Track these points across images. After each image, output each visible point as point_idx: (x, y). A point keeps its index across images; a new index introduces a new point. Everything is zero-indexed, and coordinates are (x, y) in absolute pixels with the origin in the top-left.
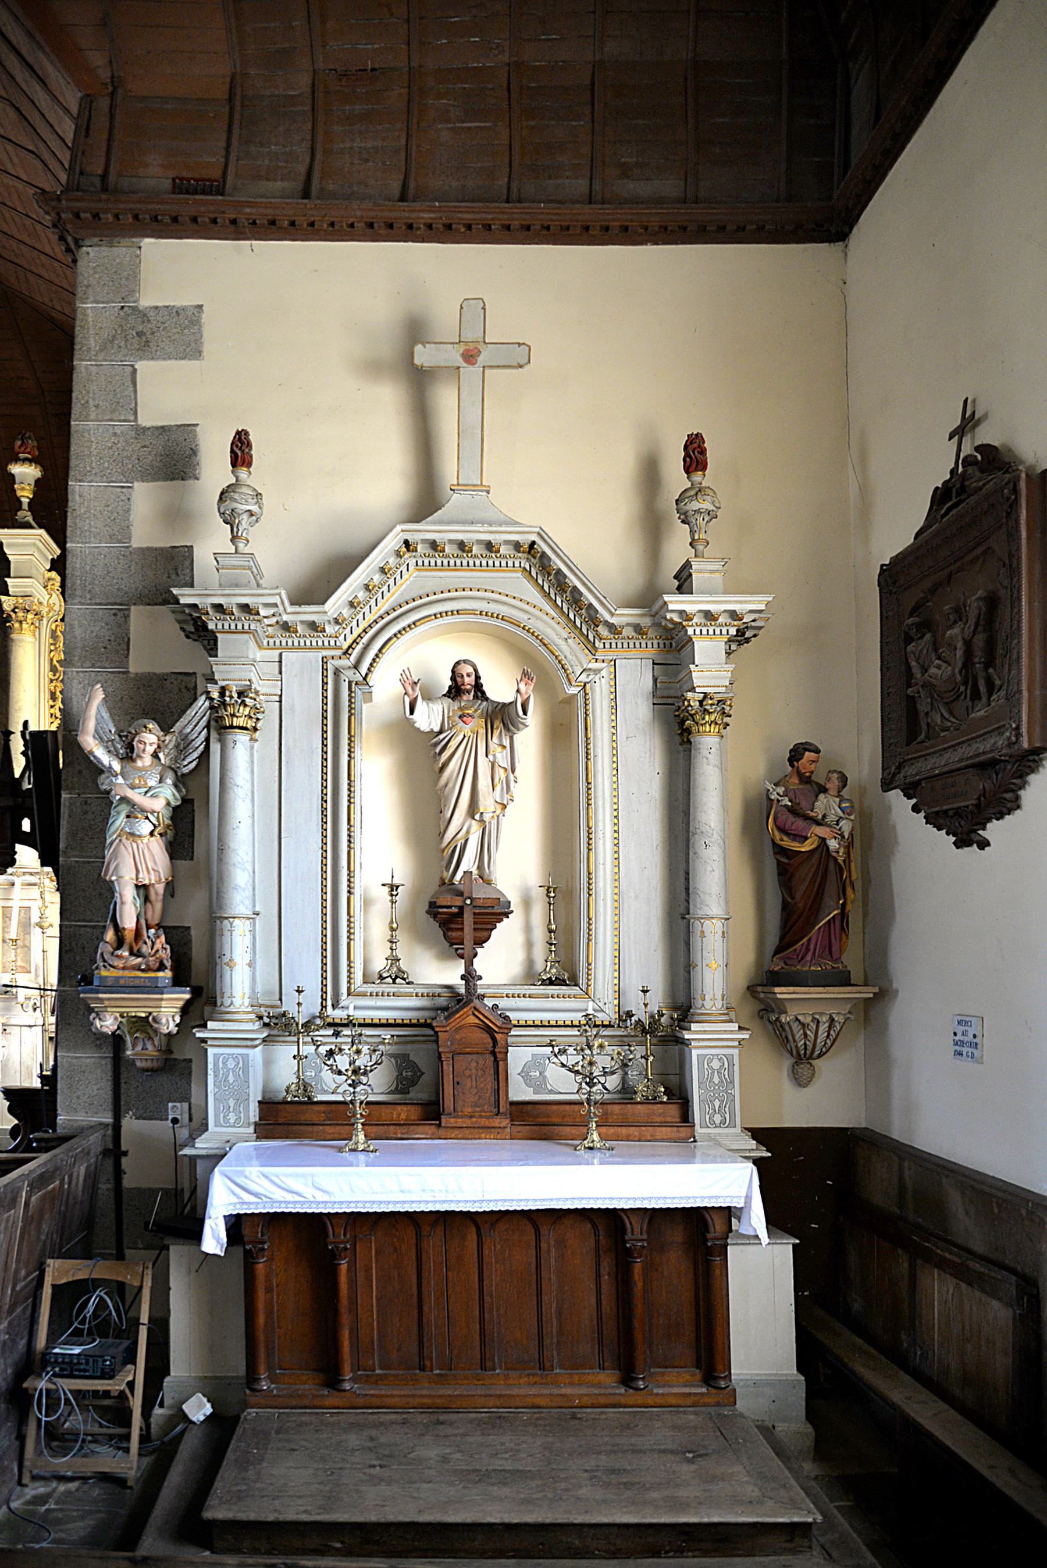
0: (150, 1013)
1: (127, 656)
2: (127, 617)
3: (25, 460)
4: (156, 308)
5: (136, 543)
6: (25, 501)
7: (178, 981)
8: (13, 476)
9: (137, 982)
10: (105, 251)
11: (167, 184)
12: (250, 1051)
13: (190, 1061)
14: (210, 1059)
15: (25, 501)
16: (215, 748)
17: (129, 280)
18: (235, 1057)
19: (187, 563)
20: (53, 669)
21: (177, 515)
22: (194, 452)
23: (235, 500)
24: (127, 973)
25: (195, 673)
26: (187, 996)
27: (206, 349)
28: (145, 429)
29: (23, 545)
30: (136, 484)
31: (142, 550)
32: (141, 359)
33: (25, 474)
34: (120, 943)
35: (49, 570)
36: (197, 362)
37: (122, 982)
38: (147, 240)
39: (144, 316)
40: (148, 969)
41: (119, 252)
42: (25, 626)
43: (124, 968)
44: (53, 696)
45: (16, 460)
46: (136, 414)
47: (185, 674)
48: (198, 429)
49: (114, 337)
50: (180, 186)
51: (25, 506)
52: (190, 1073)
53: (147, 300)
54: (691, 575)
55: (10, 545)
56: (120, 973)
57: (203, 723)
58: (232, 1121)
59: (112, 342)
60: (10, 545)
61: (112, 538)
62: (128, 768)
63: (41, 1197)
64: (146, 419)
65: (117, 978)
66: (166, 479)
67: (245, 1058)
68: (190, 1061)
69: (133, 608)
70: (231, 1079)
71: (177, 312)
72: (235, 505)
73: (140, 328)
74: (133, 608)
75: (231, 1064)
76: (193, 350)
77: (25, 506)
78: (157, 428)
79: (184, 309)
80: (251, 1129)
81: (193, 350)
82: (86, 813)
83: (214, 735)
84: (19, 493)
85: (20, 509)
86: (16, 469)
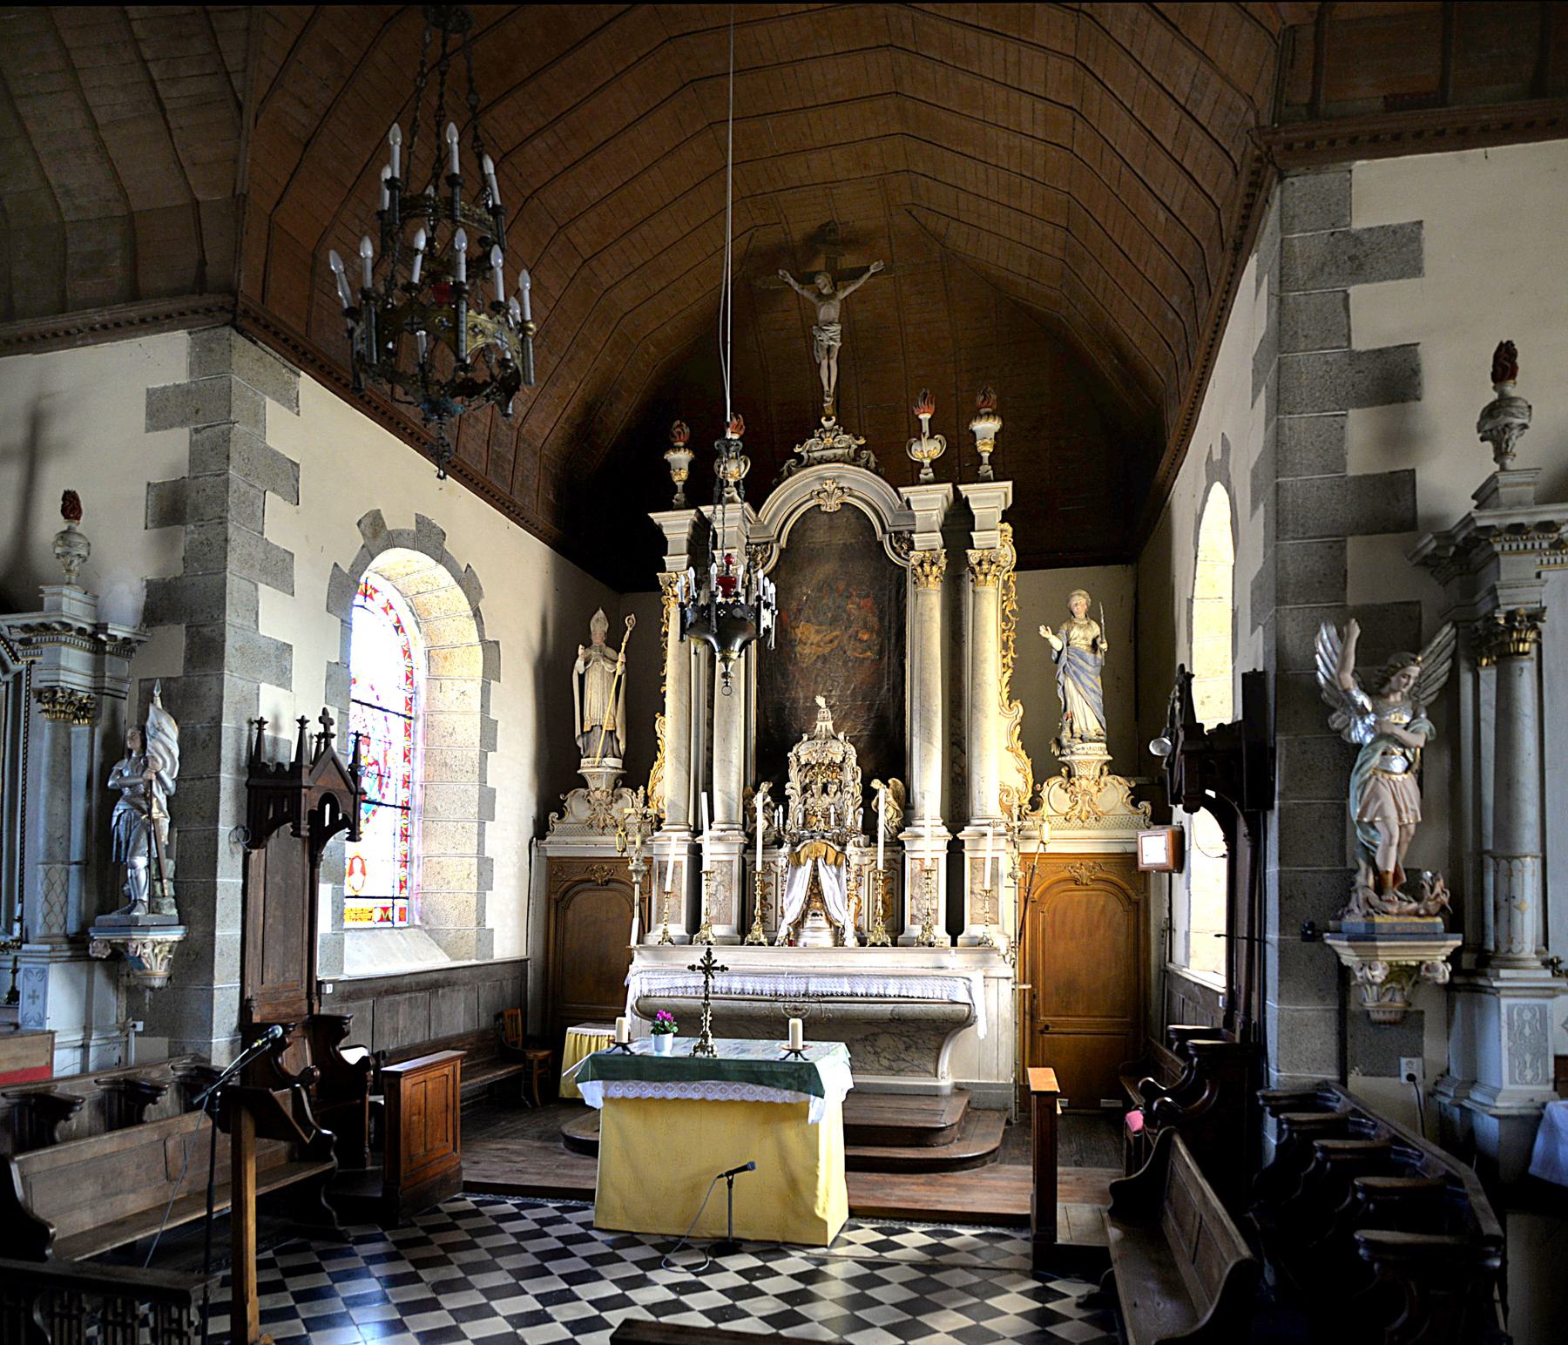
0: (1421, 963)
1: (1344, 589)
2: (1343, 549)
3: (988, 414)
4: (1370, 229)
5: (1352, 471)
6: (986, 455)
7: (1453, 926)
8: (973, 433)
9: (1414, 929)
10: (1311, 179)
11: (1379, 104)
12: (1548, 1002)
13: (1422, 1012)
14: (1504, 1010)
15: (986, 455)
16: (1467, 679)
17: (1343, 202)
18: (1531, 1008)
19: (1408, 488)
20: (1005, 619)
21: (1399, 439)
22: (1416, 372)
23: (1513, 415)
24: (1402, 919)
25: (1418, 603)
26: (1459, 943)
27: (1428, 264)
28: (1360, 354)
29: (988, 498)
30: (1351, 411)
31: (1360, 479)
32: (1354, 283)
33: (680, 460)
34: (1380, 888)
35: (1002, 522)
36: (1417, 280)
37: (1398, 929)
38: (1359, 163)
39: (1356, 239)
40: (1428, 914)
41: (1329, 178)
42: (931, 579)
43: (1398, 915)
44: (1005, 646)
45: (978, 415)
46: (1349, 339)
47: (1408, 603)
48: (1419, 348)
49: (1324, 264)
50: (1393, 104)
51: (986, 461)
52: (1422, 1027)
53: (1358, 224)
54: (1496, 489)
55: (975, 500)
56: (1395, 919)
57: (1448, 652)
58: (1529, 1078)
59: (1322, 270)
60: (975, 500)
61: (1325, 469)
62: (1381, 704)
63: (491, 1086)
64: (1358, 345)
65: (1393, 925)
66: (1383, 404)
67: (1543, 1010)
68: (1422, 1012)
69: (1349, 539)
70: (1527, 1031)
71: (1395, 231)
72: (1510, 419)
73: (1353, 251)
74: (1349, 539)
75: (1527, 1015)
76: (1413, 268)
77: (986, 461)
78: (1374, 351)
79: (1401, 227)
80: (1550, 1087)
81: (1413, 268)
82: (1305, 752)
83: (1464, 666)
84: (980, 448)
85: (981, 463)
86: (671, 456)
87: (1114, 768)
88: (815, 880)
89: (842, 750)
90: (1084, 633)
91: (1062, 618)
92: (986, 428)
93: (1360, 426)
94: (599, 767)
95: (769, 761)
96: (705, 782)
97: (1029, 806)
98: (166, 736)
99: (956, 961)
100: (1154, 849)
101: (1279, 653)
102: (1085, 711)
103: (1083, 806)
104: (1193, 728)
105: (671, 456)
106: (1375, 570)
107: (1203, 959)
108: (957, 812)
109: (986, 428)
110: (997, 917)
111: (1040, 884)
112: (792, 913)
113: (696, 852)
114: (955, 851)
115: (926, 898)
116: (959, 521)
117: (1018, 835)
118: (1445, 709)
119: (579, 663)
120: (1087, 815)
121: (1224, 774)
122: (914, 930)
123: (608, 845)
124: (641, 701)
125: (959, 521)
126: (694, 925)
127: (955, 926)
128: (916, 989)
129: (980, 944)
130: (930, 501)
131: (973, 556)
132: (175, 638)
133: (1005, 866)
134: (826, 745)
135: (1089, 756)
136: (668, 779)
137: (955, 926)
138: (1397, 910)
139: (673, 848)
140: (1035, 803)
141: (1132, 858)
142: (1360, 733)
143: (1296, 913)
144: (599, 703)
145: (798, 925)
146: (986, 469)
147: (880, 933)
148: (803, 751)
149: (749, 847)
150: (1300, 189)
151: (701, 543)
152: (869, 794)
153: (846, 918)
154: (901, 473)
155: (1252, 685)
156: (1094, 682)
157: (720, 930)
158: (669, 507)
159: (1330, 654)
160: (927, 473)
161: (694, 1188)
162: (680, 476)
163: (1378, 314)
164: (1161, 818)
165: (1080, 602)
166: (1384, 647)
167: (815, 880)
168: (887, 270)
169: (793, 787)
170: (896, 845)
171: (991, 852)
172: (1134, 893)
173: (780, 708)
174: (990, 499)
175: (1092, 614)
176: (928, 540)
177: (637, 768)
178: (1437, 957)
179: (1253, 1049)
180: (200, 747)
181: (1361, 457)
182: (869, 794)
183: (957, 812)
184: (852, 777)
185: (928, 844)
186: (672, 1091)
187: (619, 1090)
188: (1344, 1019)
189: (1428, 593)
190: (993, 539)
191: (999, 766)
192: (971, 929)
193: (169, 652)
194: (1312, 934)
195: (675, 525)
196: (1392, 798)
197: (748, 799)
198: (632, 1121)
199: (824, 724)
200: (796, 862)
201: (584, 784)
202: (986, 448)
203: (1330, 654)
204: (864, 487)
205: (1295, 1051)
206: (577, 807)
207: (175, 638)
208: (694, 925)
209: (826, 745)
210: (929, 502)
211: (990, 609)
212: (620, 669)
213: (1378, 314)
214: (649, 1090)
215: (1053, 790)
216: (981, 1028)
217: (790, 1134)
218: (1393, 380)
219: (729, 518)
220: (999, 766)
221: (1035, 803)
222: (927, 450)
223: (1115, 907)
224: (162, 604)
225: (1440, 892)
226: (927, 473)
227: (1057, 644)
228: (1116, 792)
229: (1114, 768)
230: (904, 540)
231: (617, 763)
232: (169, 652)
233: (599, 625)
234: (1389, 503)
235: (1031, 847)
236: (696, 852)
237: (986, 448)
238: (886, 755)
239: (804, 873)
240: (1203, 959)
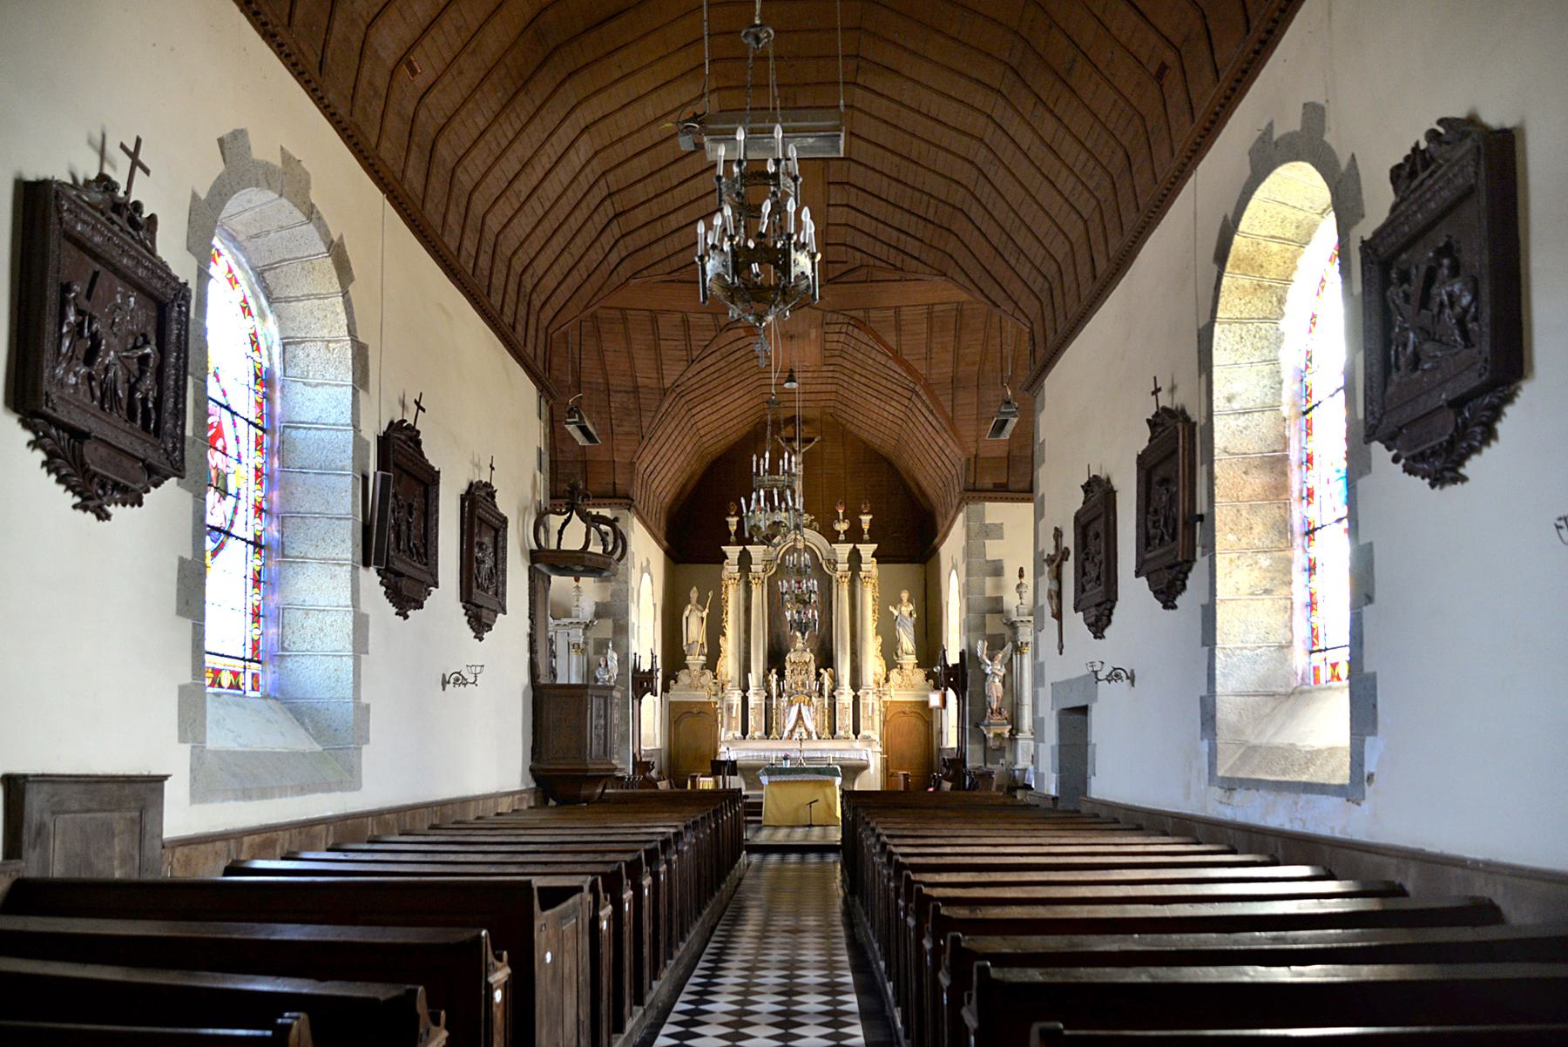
17: (982, 516)
21: (998, 587)
41: (980, 506)
86: (729, 519)
87: (919, 666)
88: (800, 712)
89: (809, 656)
90: (907, 609)
91: (898, 602)
92: (866, 519)
93: (989, 581)
94: (695, 660)
95: (776, 658)
96: (746, 669)
97: (887, 685)
98: (613, 657)
99: (858, 744)
100: (935, 700)
101: (969, 646)
102: (907, 642)
103: (906, 682)
104: (946, 665)
105: (729, 519)
106: (994, 625)
107: (951, 740)
108: (856, 684)
109: (866, 519)
110: (872, 728)
111: (890, 715)
112: (789, 727)
113: (745, 700)
114: (856, 699)
115: (845, 720)
116: (855, 558)
117: (880, 694)
118: (1009, 665)
119: (686, 613)
120: (908, 686)
121: (959, 678)
122: (840, 733)
123: (701, 696)
124: (715, 630)
125: (855, 558)
126: (745, 732)
127: (856, 732)
128: (847, 755)
129: (867, 738)
130: (843, 550)
131: (862, 574)
132: (609, 623)
133: (876, 707)
134: (801, 654)
135: (909, 660)
136: (729, 665)
137: (856, 732)
138: (996, 718)
139: (736, 698)
140: (887, 680)
141: (926, 703)
142: (988, 671)
143: (972, 721)
144: (694, 629)
145: (792, 731)
146: (866, 537)
147: (826, 734)
148: (791, 656)
149: (769, 697)
150: (972, 507)
151: (745, 561)
152: (818, 675)
153: (811, 725)
154: (833, 537)
155: (962, 654)
156: (911, 630)
157: (757, 734)
158: (728, 544)
159: (981, 648)
160: (842, 537)
161: (797, 810)
162: (733, 528)
163: (993, 550)
164: (936, 688)
165: (905, 595)
166: (995, 644)
167: (800, 712)
168: (822, 440)
169: (787, 673)
170: (832, 697)
171: (870, 700)
172: (926, 716)
173: (778, 636)
174: (867, 550)
175: (909, 600)
176: (843, 567)
177: (712, 662)
178: (1006, 731)
179: (962, 761)
180: (623, 661)
181: (989, 593)
182: (818, 675)
183: (856, 684)
184: (813, 668)
185: (845, 697)
186: (792, 778)
187: (774, 779)
188: (986, 749)
189: (1008, 632)
190: (869, 566)
191: (873, 664)
192: (863, 732)
193: (605, 629)
194: (977, 726)
195: (733, 552)
196: (995, 689)
197: (765, 677)
198: (776, 790)
199: (799, 645)
200: (791, 704)
201: (687, 667)
202: (866, 527)
203: (981, 648)
204: (814, 538)
205: (973, 761)
206: (683, 676)
207: (609, 623)
208: (745, 732)
209: (801, 654)
210: (843, 550)
211: (868, 597)
212: (705, 614)
213: (993, 550)
214: (784, 778)
215: (894, 674)
216: (872, 769)
217: (828, 791)
218: (997, 570)
219: (756, 551)
220: (873, 664)
221: (887, 680)
222: (842, 527)
223: (920, 724)
224: (601, 611)
225: (1005, 713)
226: (842, 537)
227: (896, 613)
228: (920, 675)
229: (919, 666)
230: (833, 563)
231: (703, 658)
232: (605, 629)
233: (694, 594)
234: (996, 606)
235: (887, 698)
236: (745, 700)
237: (866, 527)
238: (826, 659)
239: (795, 710)
240: (951, 740)
